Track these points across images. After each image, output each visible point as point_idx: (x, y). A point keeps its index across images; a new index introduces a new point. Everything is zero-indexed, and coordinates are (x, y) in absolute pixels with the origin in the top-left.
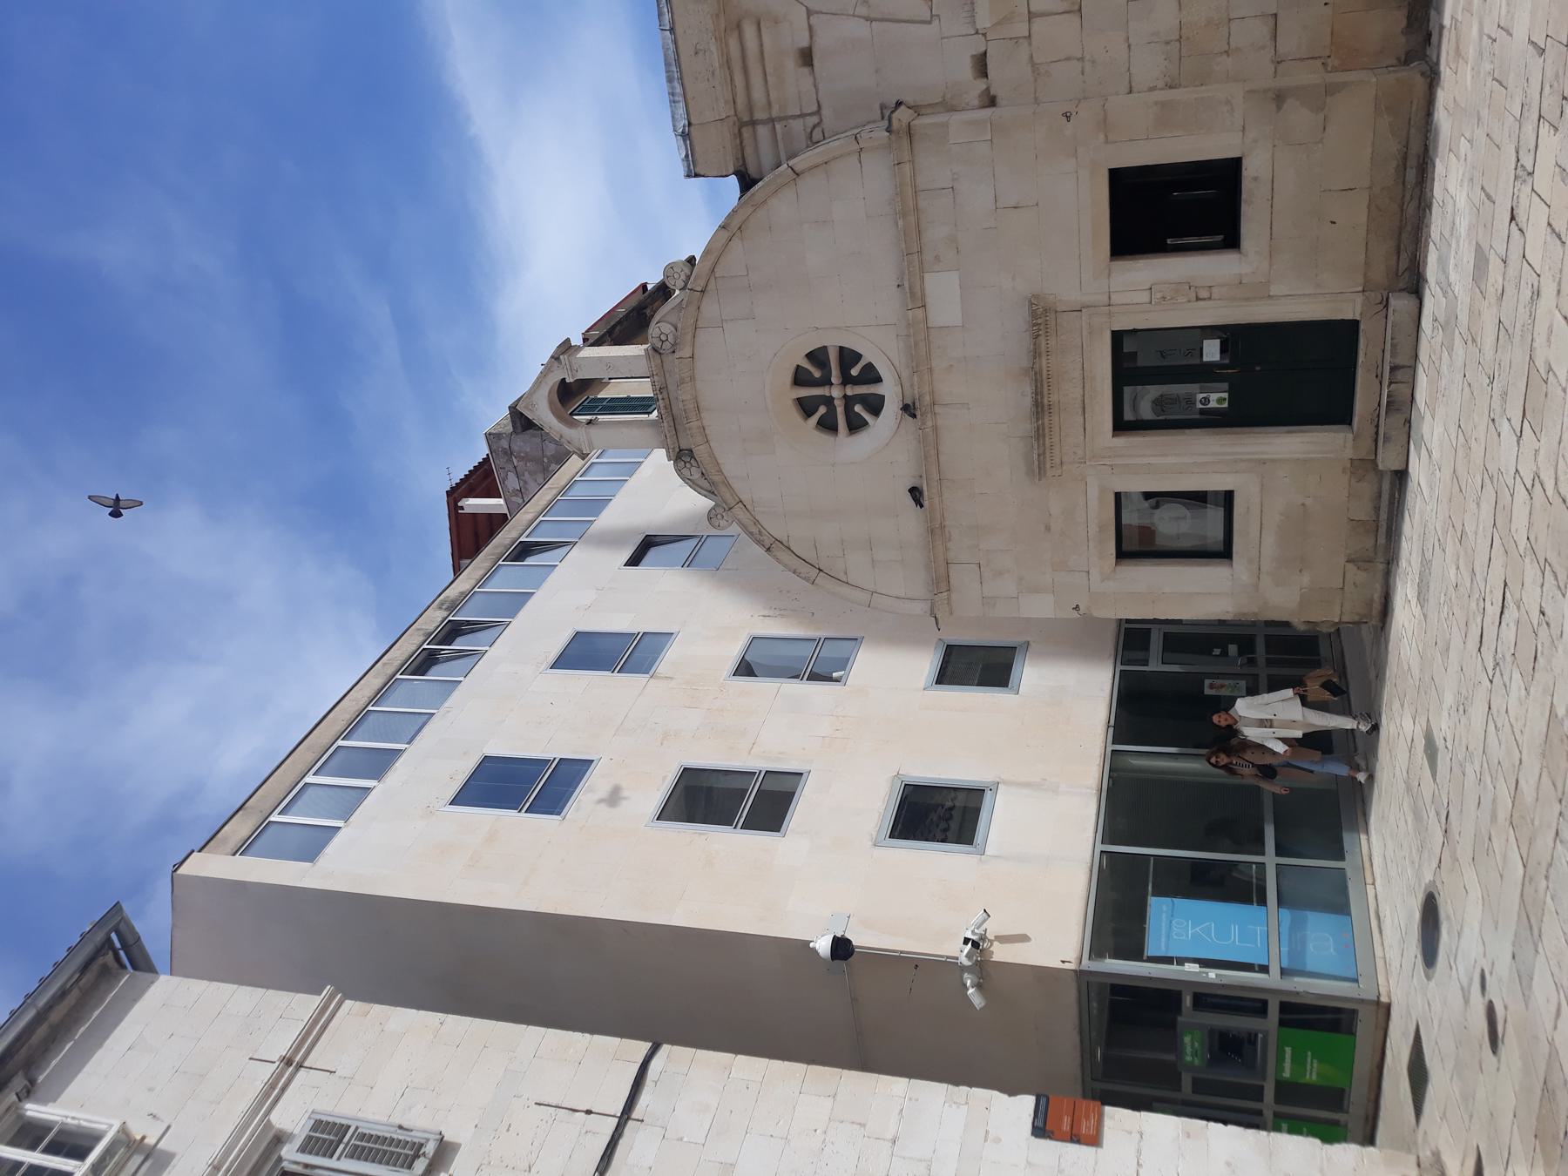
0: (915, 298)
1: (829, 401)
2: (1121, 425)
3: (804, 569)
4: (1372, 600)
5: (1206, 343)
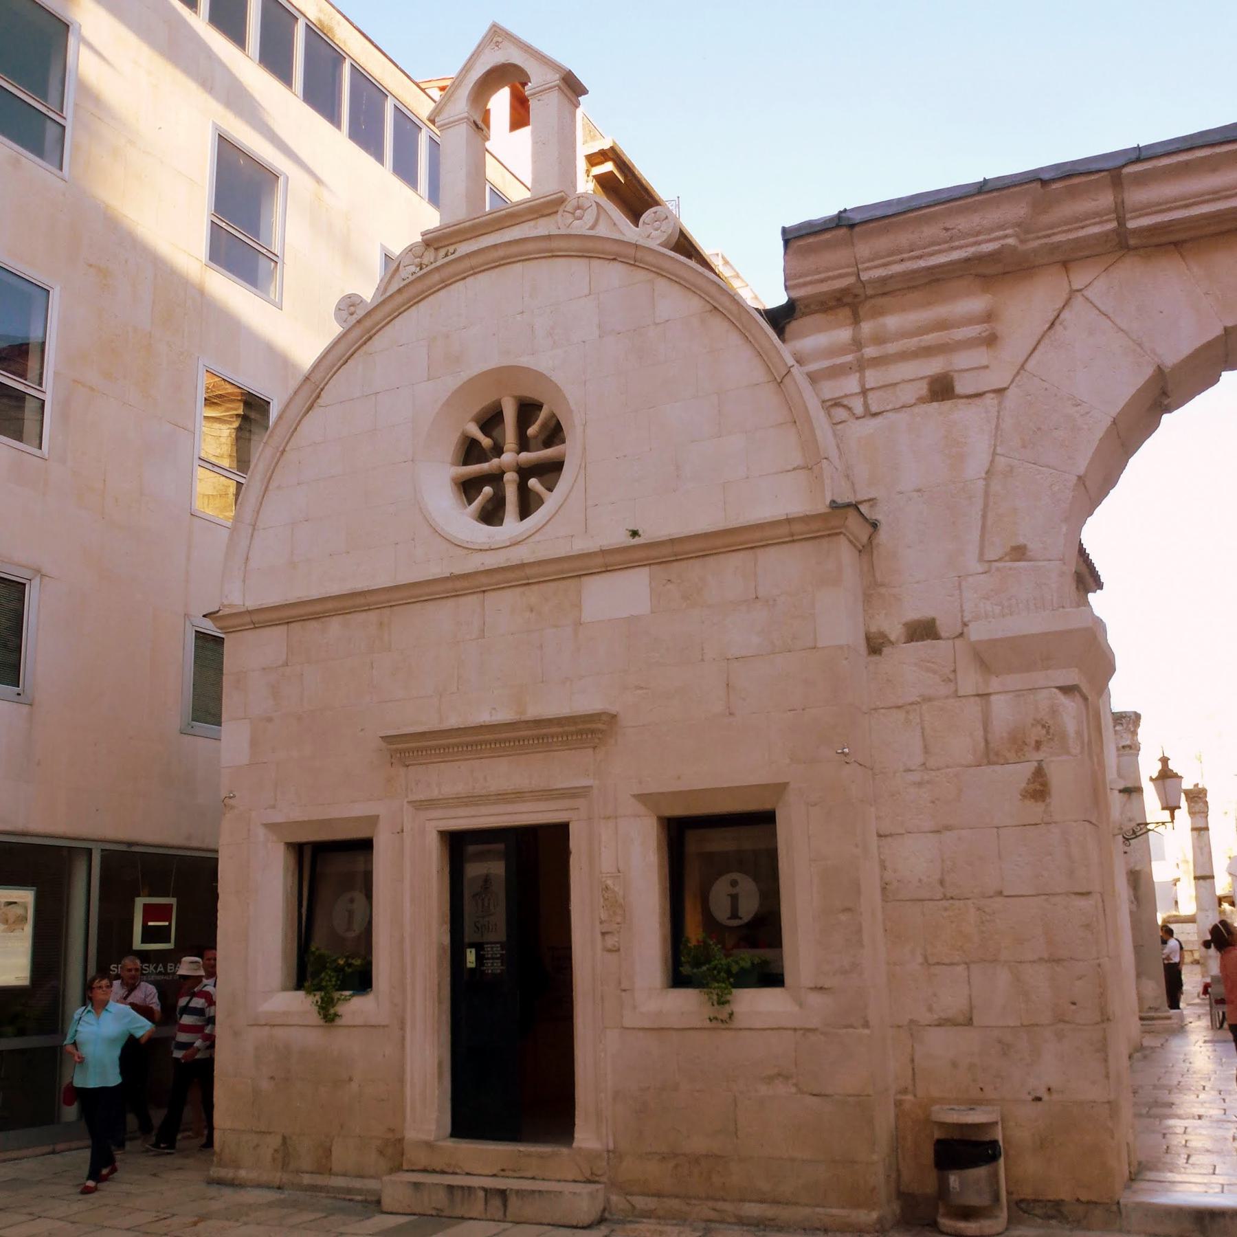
0: (610, 561)
1: (498, 450)
4: (238, 1167)
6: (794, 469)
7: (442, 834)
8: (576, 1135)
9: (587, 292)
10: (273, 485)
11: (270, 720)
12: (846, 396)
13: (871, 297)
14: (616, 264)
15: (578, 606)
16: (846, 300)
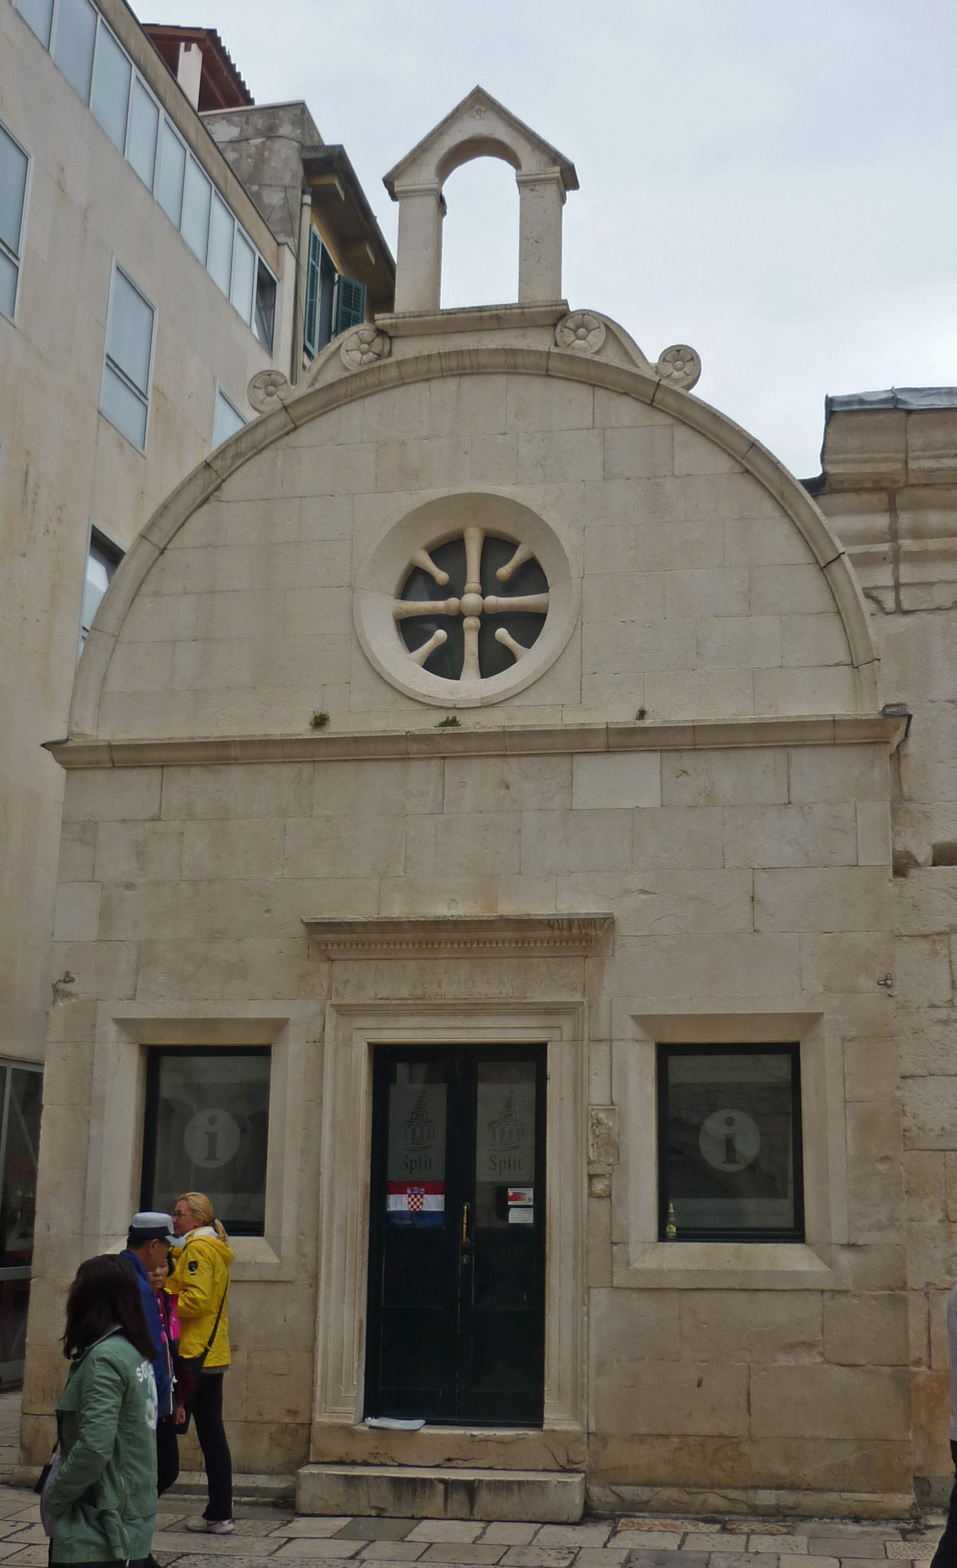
1: (455, 589)
2: (385, 1058)
3: (167, 524)
5: (441, 1198)
6: (836, 665)
7: (369, 1044)
8: (545, 1415)
9: (589, 423)
10: (146, 589)
11: (130, 886)
12: (876, 588)
13: (913, 486)
14: (627, 400)
15: (570, 786)
16: (884, 484)
